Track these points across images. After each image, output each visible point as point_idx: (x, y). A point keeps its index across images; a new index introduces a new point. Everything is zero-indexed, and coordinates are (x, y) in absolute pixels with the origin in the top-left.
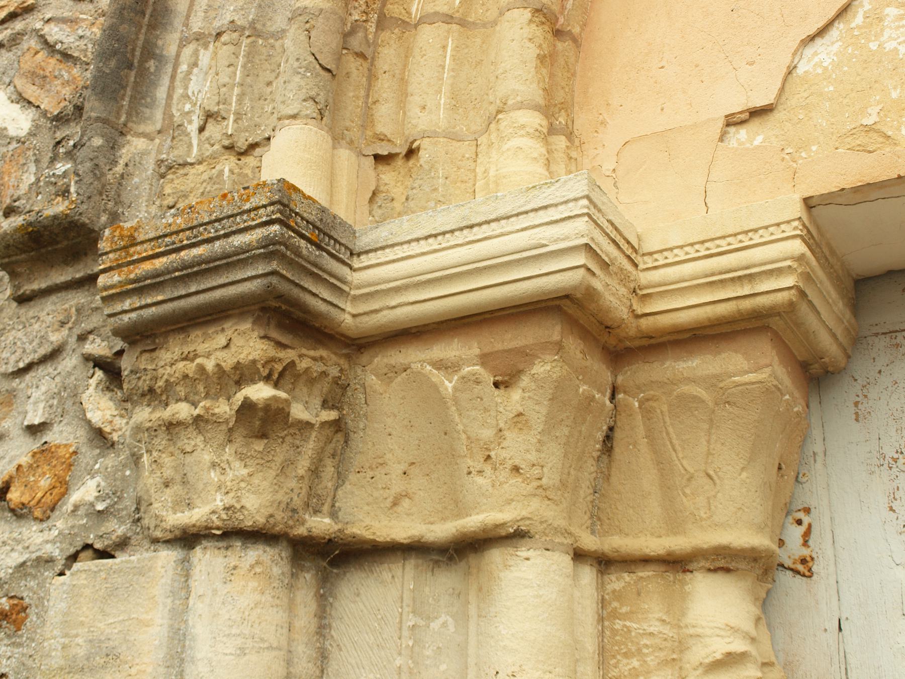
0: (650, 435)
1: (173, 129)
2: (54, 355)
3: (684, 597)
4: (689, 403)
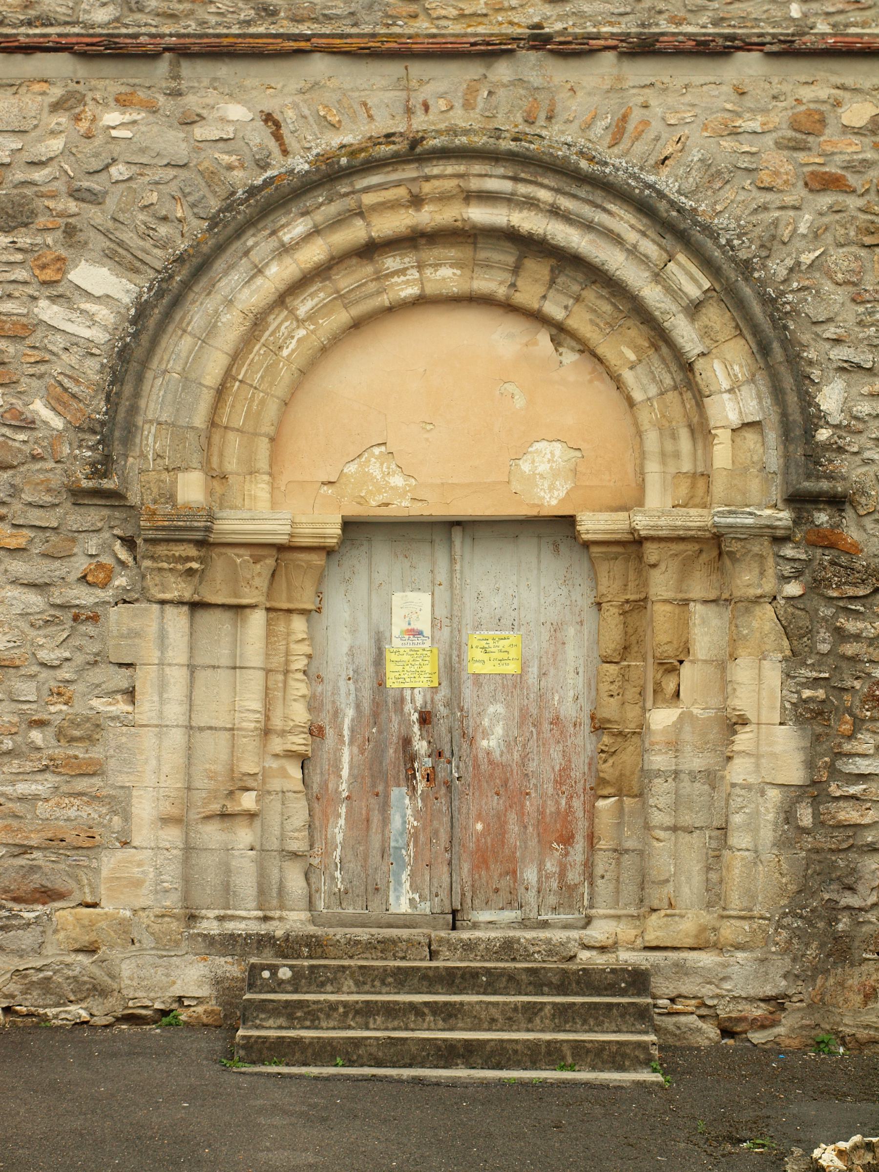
0: (286, 575)
1: (143, 456)
2: (98, 531)
3: (290, 620)
4: (299, 567)
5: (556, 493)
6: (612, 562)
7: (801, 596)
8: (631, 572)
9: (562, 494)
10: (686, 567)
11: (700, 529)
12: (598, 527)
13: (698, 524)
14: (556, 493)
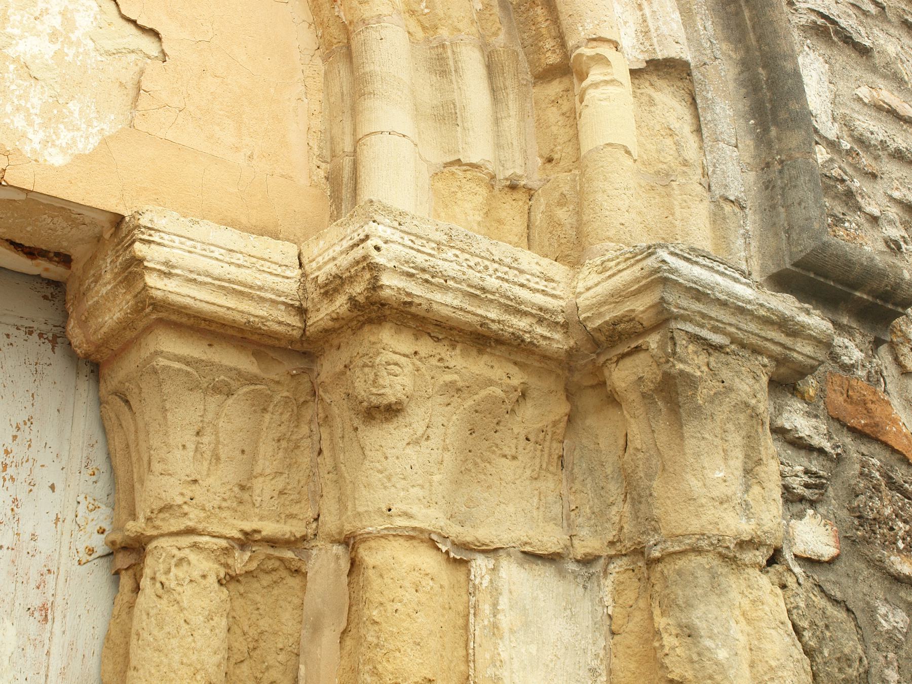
5: (65, 137)
6: (213, 401)
7: (832, 561)
8: (266, 448)
9: (88, 144)
10: (485, 424)
11: (542, 316)
12: (203, 264)
13: (540, 299)
14: (65, 137)
